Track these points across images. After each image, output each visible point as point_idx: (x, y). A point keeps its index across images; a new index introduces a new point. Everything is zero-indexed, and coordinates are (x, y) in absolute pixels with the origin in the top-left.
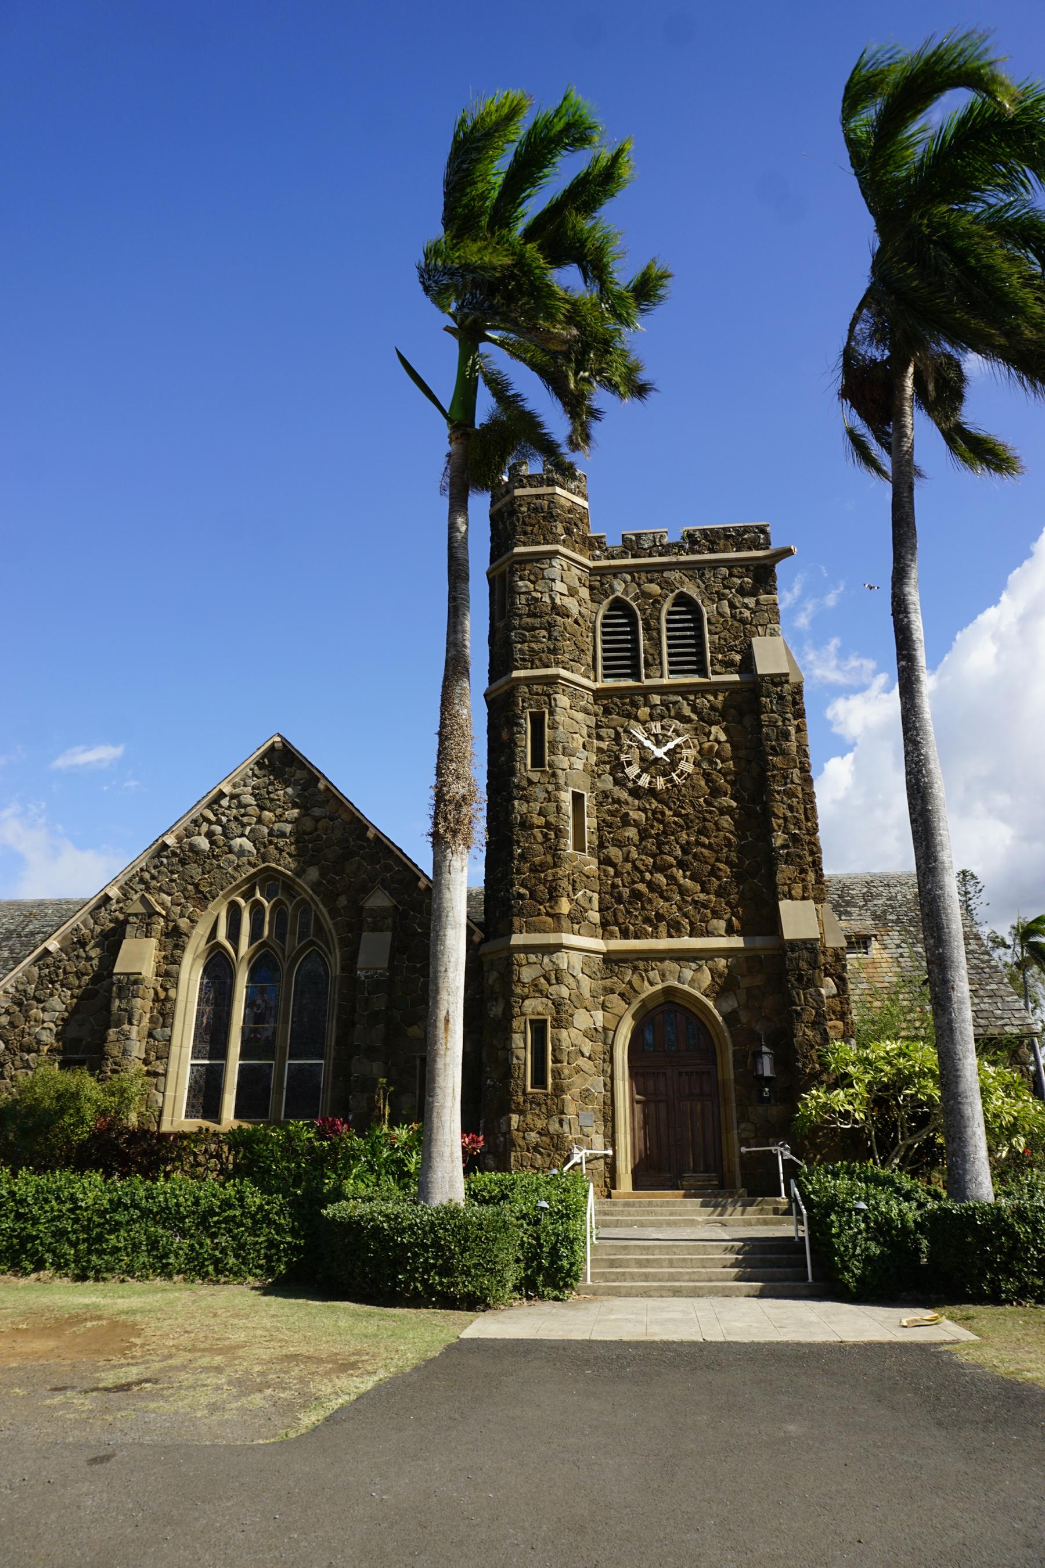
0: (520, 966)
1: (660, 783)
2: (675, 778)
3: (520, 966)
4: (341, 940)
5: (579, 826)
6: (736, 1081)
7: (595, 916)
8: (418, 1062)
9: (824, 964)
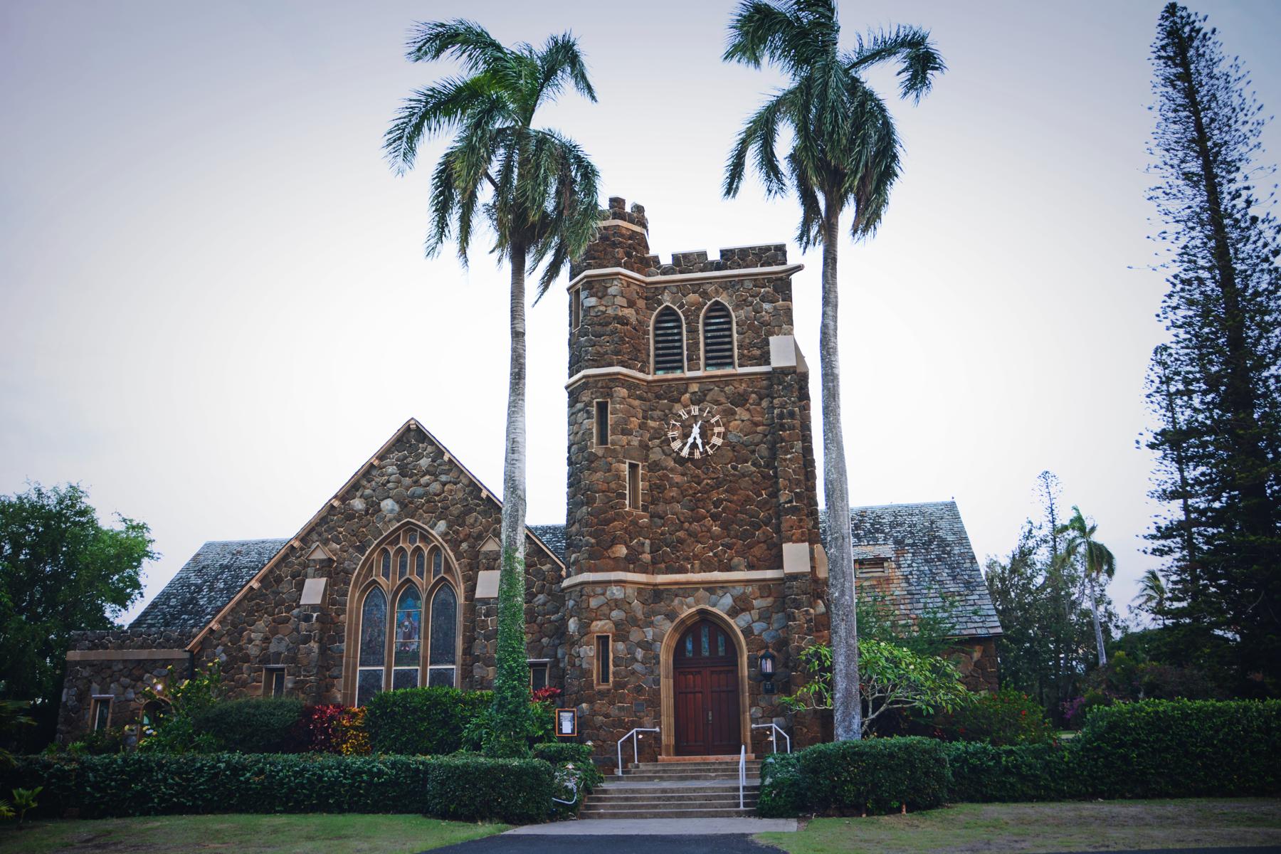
0: (589, 596)
4: (464, 576)
6: (749, 677)
7: (646, 557)
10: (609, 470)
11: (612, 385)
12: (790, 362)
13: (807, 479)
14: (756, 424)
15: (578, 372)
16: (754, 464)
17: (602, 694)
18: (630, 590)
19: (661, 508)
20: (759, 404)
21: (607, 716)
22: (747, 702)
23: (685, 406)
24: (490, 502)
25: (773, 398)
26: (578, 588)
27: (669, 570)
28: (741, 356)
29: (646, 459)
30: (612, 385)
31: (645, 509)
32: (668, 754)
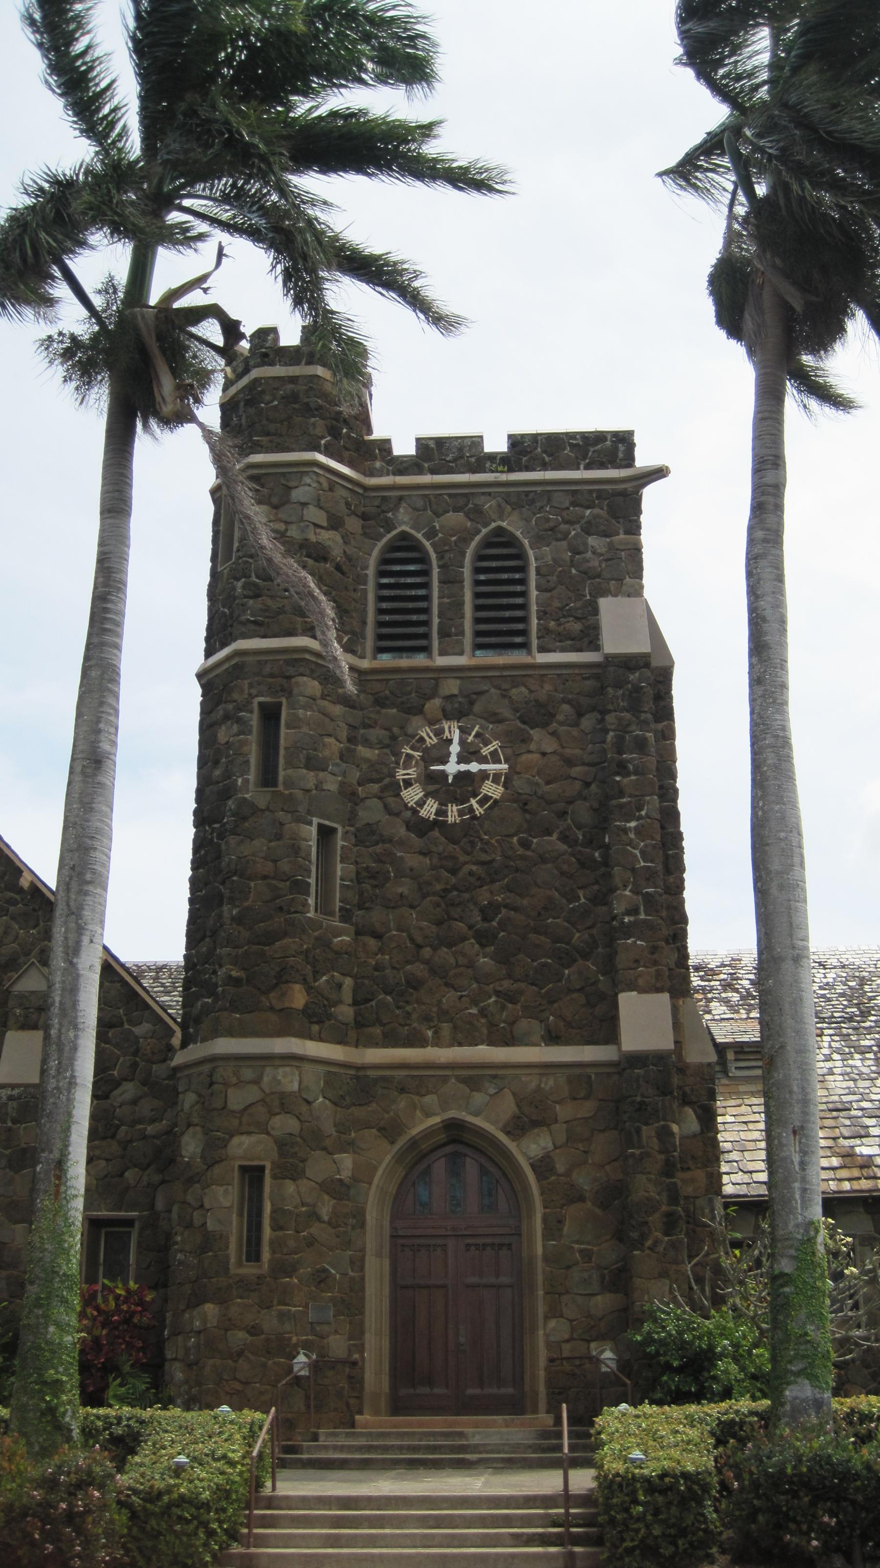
0: (227, 1085)
1: (453, 814)
2: (476, 806)
3: (227, 1085)
5: (325, 877)
6: (546, 1259)
7: (345, 1012)
9: (680, 1088)
10: (278, 837)
11: (291, 671)
12: (642, 646)
13: (668, 871)
14: (570, 762)
15: (224, 645)
16: (564, 838)
17: (245, 1286)
18: (313, 1077)
19: (377, 916)
20: (576, 724)
21: (254, 1330)
22: (541, 1309)
23: (431, 723)
24: (37, 890)
25: (604, 712)
26: (206, 1068)
27: (391, 1040)
28: (544, 632)
29: (351, 818)
30: (291, 671)
31: (346, 916)
32: (377, 1413)
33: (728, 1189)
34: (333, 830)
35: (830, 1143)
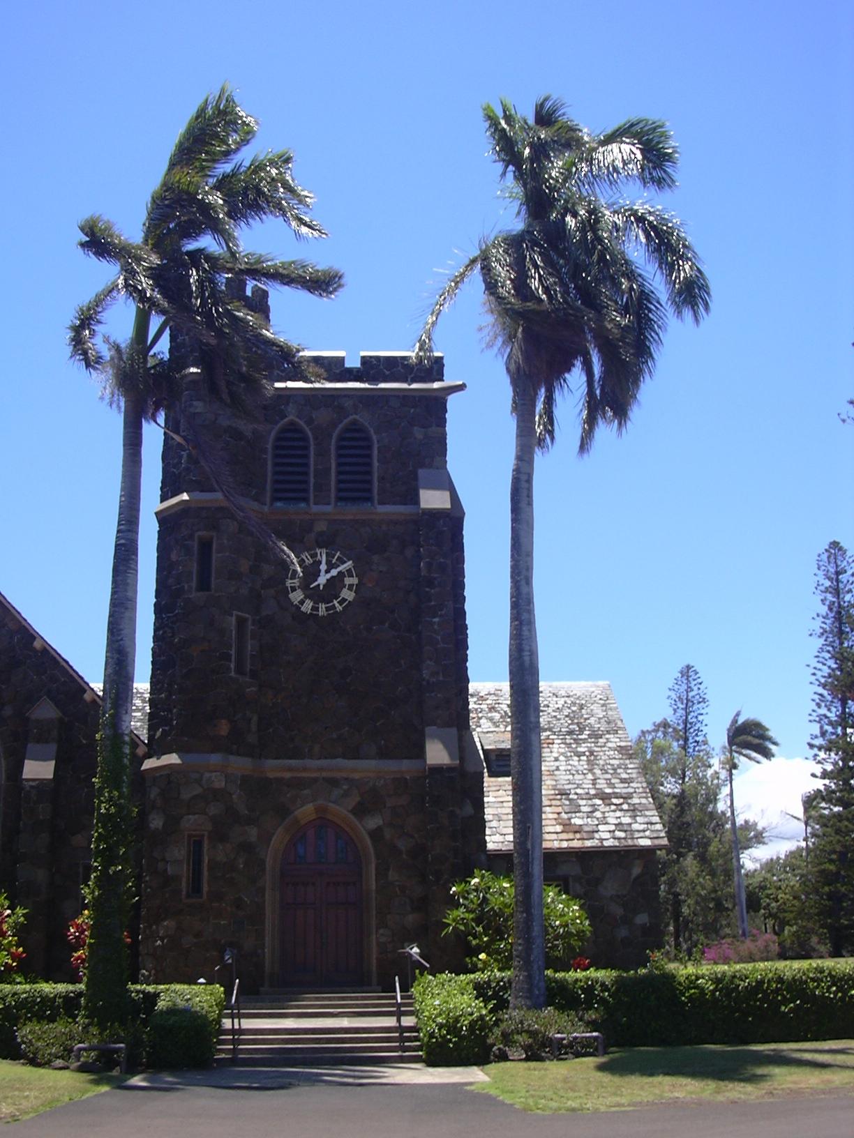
1: (322, 610)
8: (81, 870)
22: (374, 922)
25: (419, 546)
33: (490, 846)
34: (246, 620)
35: (556, 816)
